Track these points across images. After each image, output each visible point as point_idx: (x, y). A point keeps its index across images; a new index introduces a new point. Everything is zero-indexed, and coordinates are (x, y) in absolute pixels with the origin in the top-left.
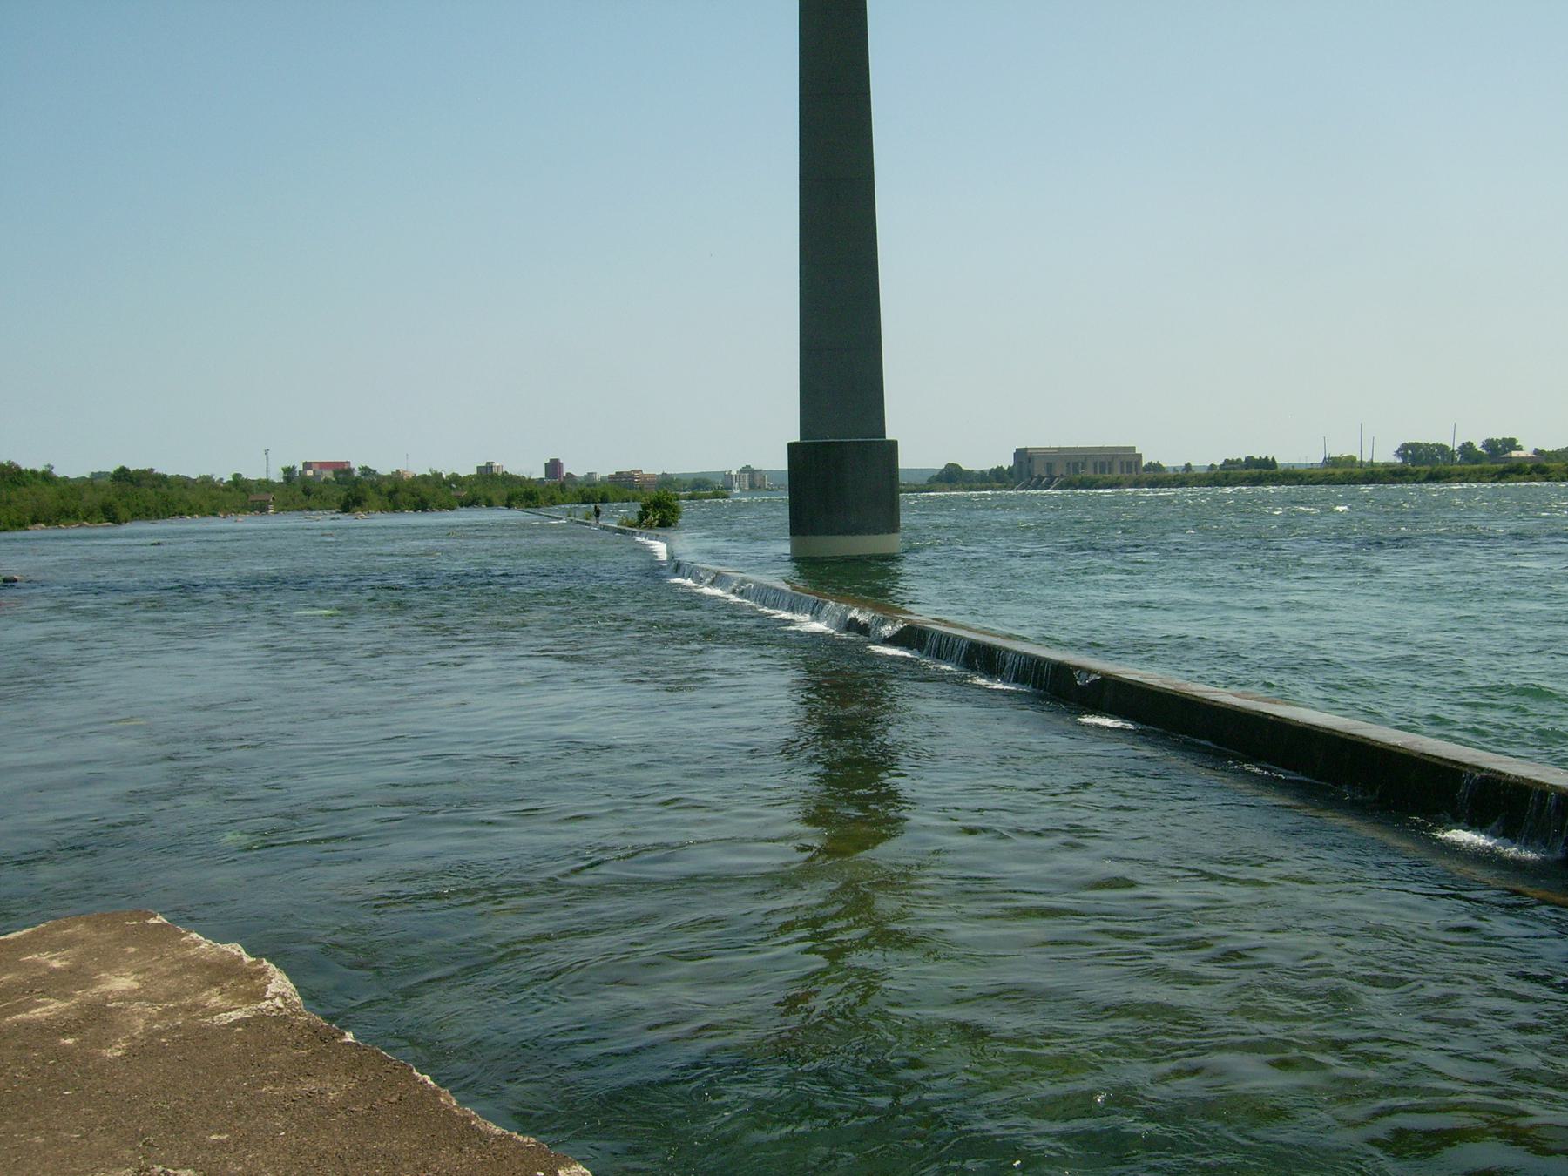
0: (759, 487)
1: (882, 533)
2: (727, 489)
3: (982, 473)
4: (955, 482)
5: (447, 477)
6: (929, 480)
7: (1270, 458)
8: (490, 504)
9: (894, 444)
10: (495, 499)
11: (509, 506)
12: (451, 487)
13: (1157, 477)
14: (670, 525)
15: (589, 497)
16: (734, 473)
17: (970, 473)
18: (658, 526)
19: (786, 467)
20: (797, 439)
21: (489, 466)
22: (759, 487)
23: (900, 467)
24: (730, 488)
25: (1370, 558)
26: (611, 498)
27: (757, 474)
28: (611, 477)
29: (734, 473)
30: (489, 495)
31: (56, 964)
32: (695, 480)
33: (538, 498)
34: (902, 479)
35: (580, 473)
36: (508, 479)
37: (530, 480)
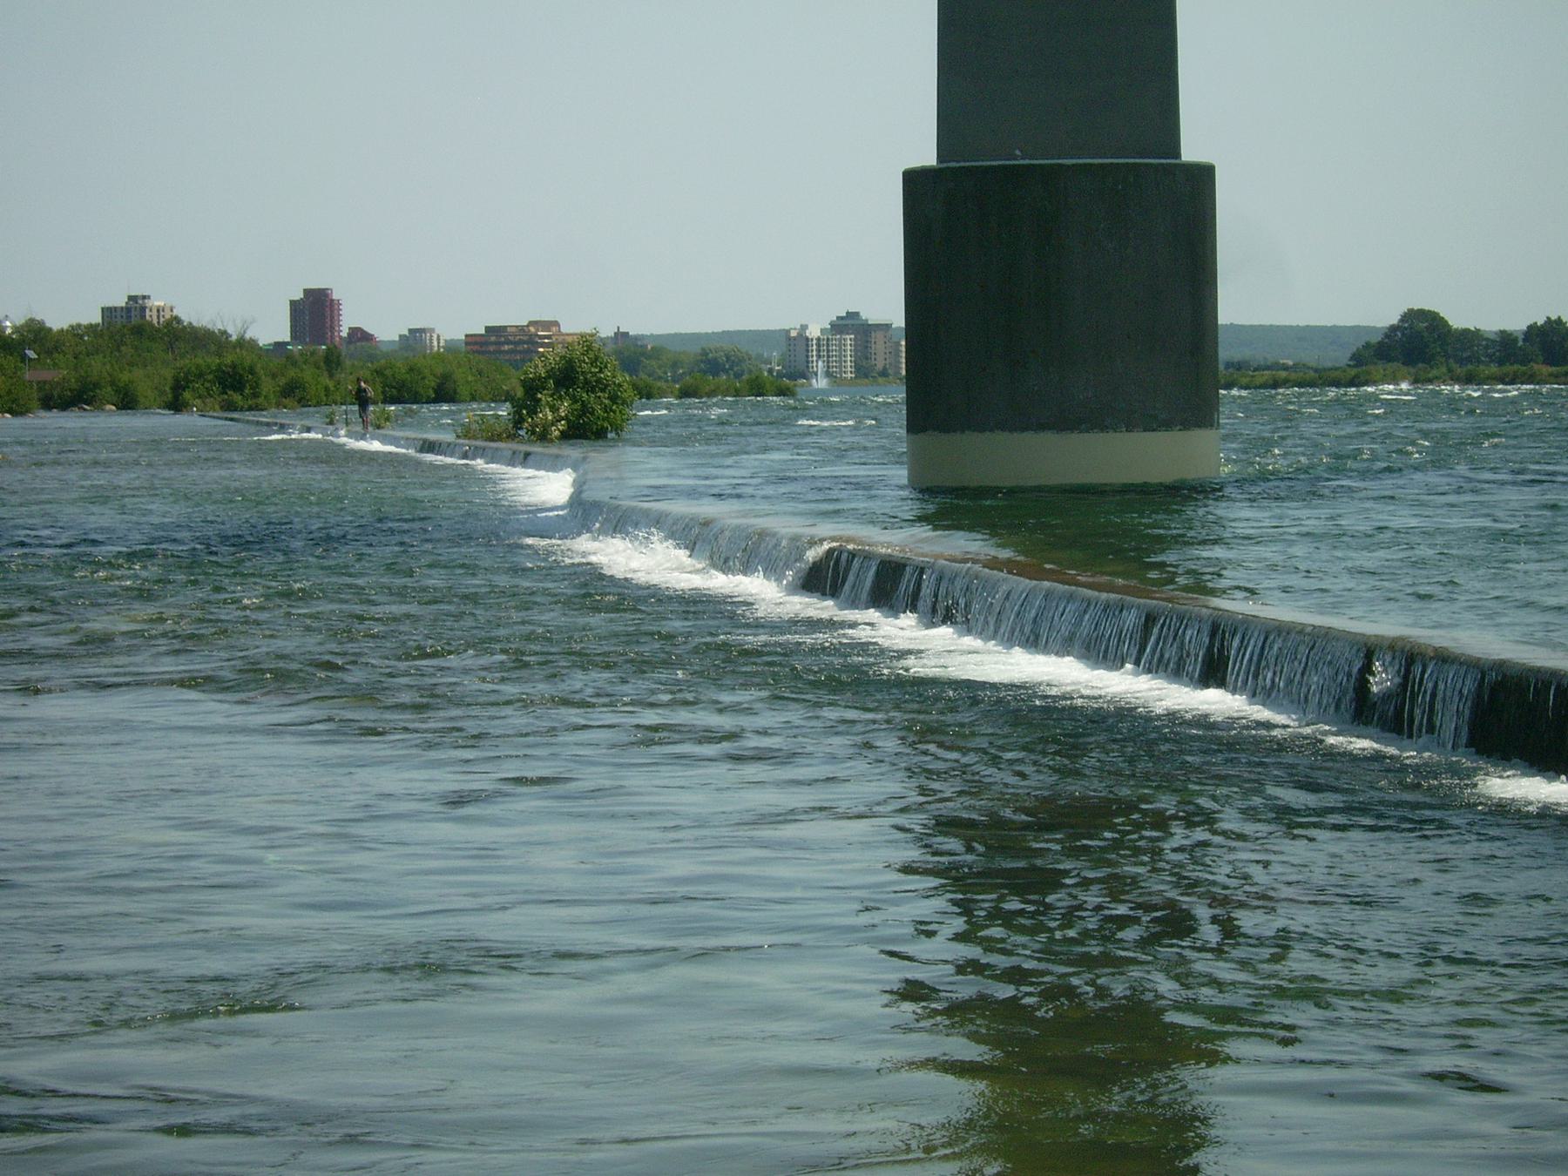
0: (884, 373)
1: (1167, 425)
2: (793, 376)
3: (1506, 339)
4: (1429, 360)
5: (16, 329)
6: (1354, 357)
7: (406, 333)
8: (127, 402)
9: (1203, 176)
10: (144, 389)
11: (176, 405)
12: (24, 358)
13: (606, 789)
14: (600, 434)
15: (401, 386)
16: (814, 332)
17: (1469, 338)
18: (565, 436)
19: (903, 325)
20: (927, 156)
21: (136, 304)
22: (884, 373)
23: (1222, 319)
24: (805, 374)
25: (923, 858)
26: (464, 391)
27: (878, 337)
28: (471, 340)
29: (814, 332)
30: (125, 377)
31: (1475, 395)
32: (704, 353)
33: (256, 386)
34: (1226, 352)
35: (387, 330)
36: (177, 335)
37: (245, 344)
